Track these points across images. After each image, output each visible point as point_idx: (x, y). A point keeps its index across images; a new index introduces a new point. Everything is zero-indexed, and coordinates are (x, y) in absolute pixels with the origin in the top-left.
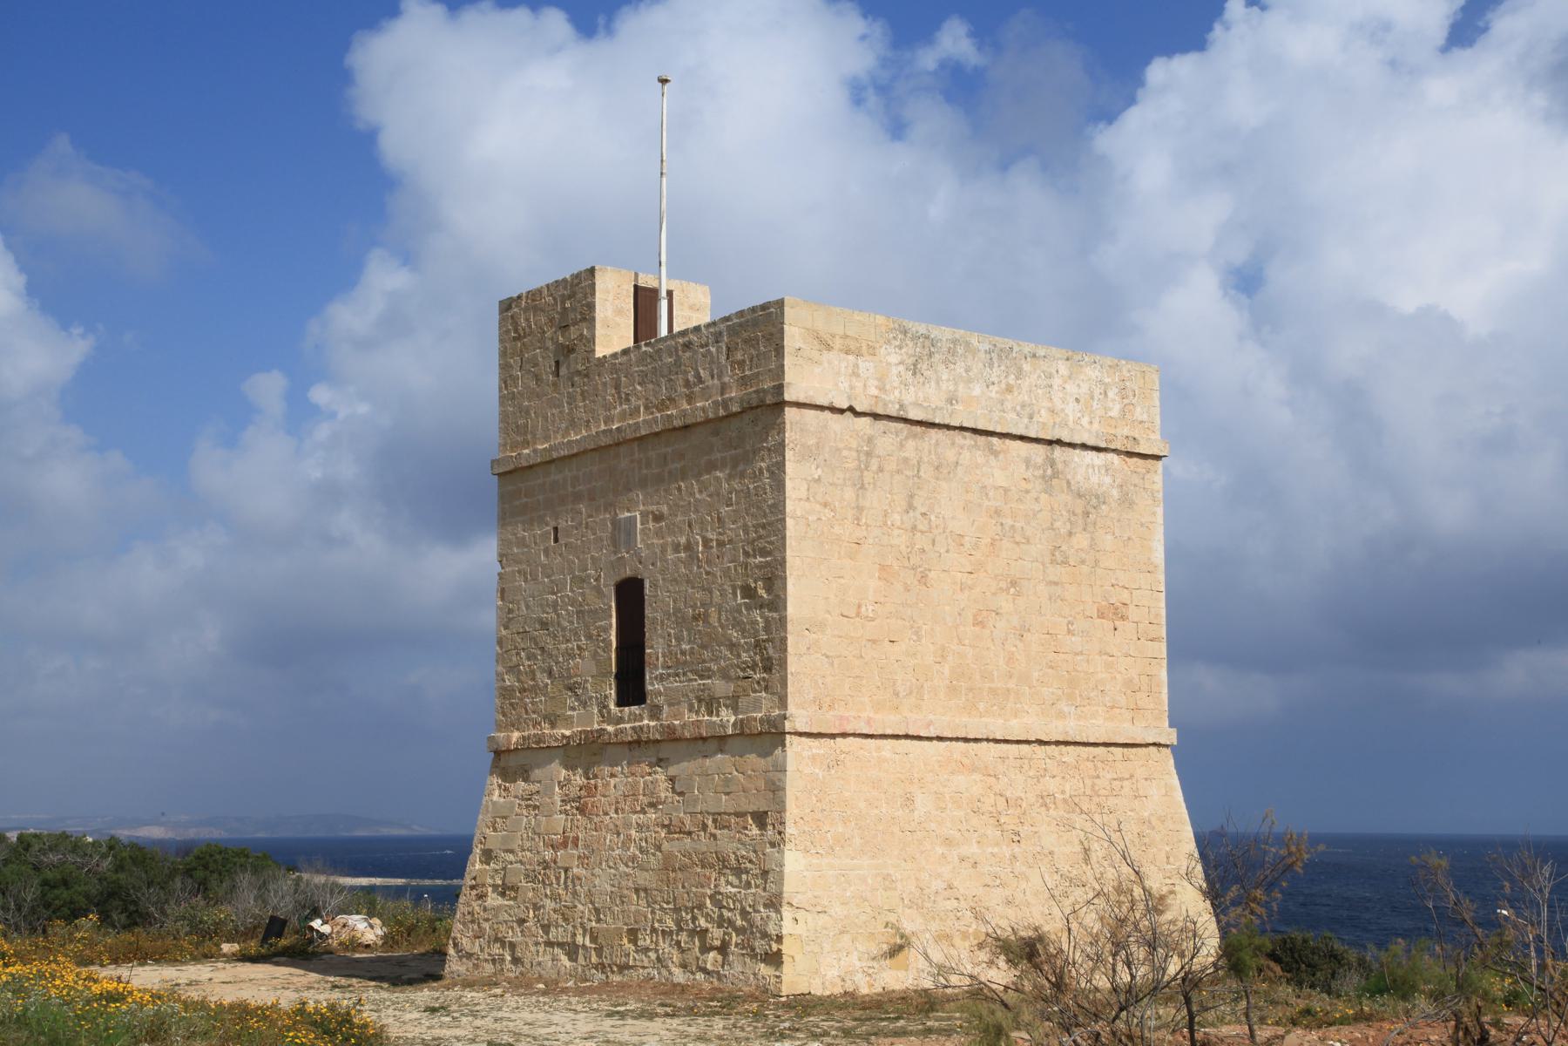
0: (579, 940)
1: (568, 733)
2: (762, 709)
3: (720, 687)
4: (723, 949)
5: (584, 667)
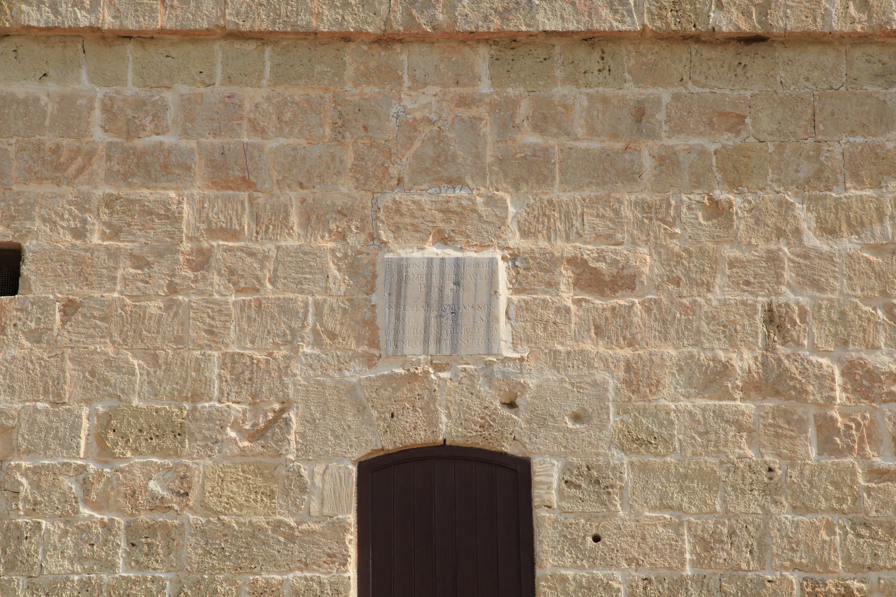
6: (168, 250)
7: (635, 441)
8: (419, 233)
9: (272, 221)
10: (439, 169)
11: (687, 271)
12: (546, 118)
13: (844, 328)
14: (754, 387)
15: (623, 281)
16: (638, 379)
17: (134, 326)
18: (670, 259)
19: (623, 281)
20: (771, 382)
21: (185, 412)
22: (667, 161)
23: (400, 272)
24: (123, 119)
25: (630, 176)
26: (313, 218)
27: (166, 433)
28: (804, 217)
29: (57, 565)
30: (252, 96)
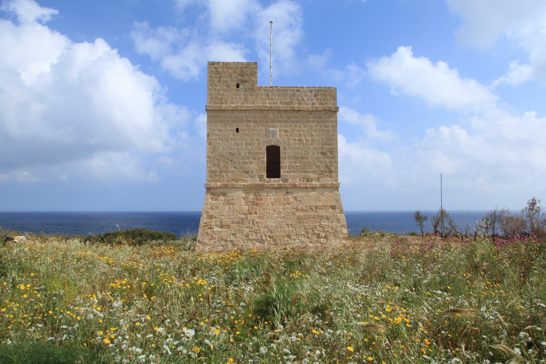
1: (246, 184)
2: (328, 181)
3: (312, 176)
4: (326, 237)
6: (250, 129)
7: (288, 145)
8: (271, 127)
9: (259, 126)
10: (273, 121)
11: (293, 131)
12: (282, 117)
13: (305, 136)
14: (298, 141)
15: (288, 131)
16: (289, 140)
17: (248, 135)
18: (291, 129)
19: (288, 131)
20: (299, 140)
21: (491, 317)
22: (291, 121)
23: (269, 131)
24: (246, 117)
25: (288, 122)
26: (262, 126)
27: (251, 144)
28: (302, 126)
29: (243, 155)
30: (257, 115)
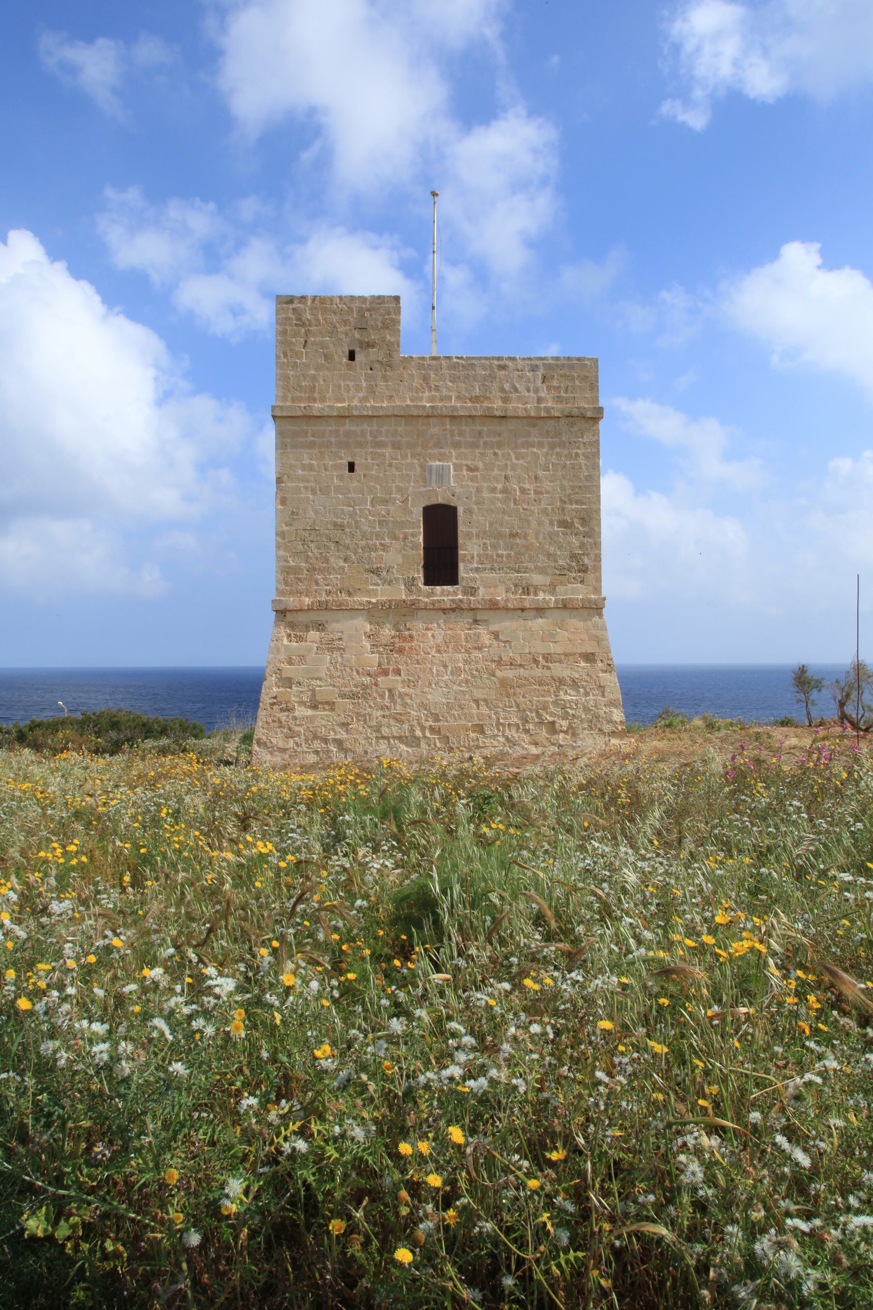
0: (418, 733)
1: (374, 600)
2: (577, 592)
3: (537, 579)
5: (392, 557)
